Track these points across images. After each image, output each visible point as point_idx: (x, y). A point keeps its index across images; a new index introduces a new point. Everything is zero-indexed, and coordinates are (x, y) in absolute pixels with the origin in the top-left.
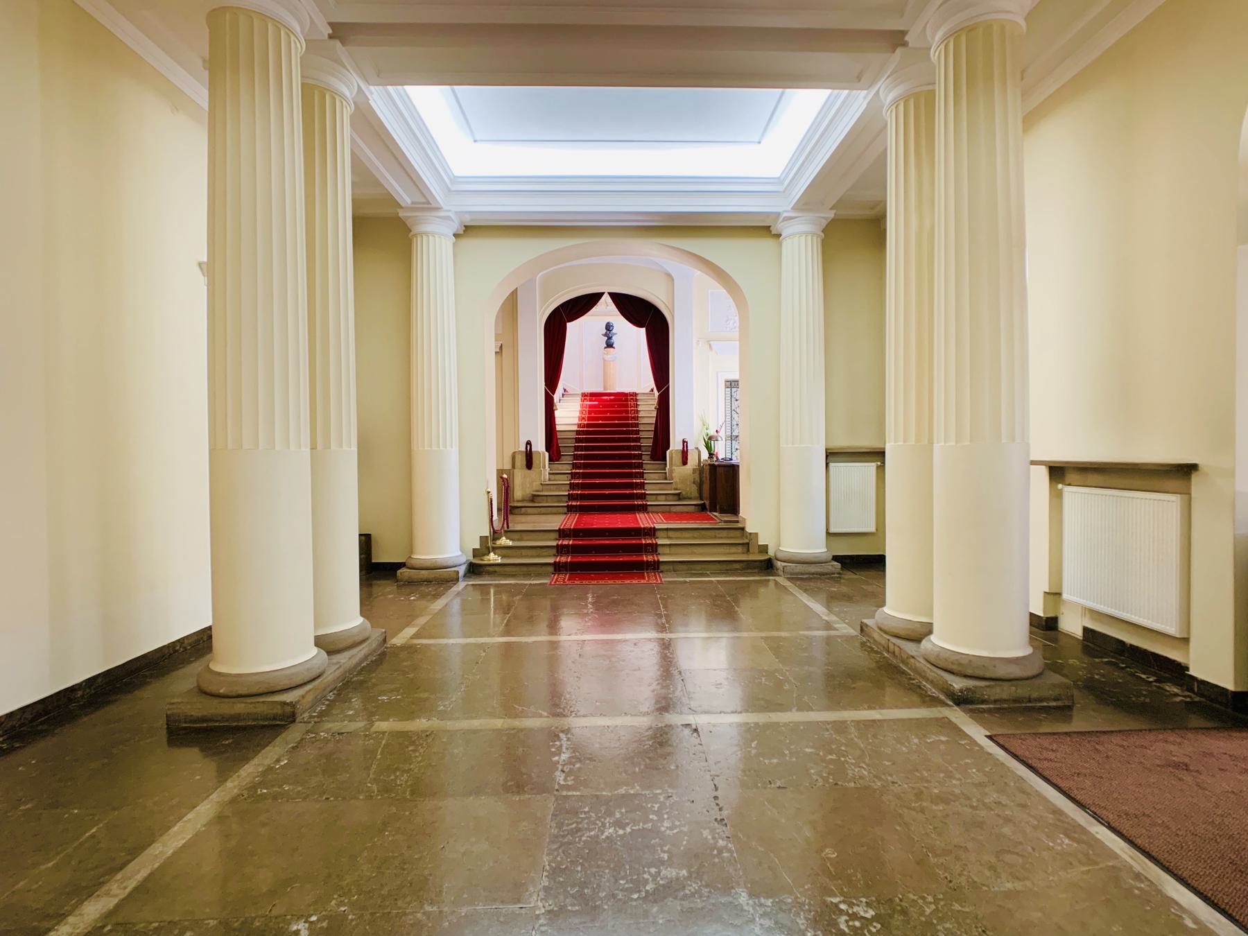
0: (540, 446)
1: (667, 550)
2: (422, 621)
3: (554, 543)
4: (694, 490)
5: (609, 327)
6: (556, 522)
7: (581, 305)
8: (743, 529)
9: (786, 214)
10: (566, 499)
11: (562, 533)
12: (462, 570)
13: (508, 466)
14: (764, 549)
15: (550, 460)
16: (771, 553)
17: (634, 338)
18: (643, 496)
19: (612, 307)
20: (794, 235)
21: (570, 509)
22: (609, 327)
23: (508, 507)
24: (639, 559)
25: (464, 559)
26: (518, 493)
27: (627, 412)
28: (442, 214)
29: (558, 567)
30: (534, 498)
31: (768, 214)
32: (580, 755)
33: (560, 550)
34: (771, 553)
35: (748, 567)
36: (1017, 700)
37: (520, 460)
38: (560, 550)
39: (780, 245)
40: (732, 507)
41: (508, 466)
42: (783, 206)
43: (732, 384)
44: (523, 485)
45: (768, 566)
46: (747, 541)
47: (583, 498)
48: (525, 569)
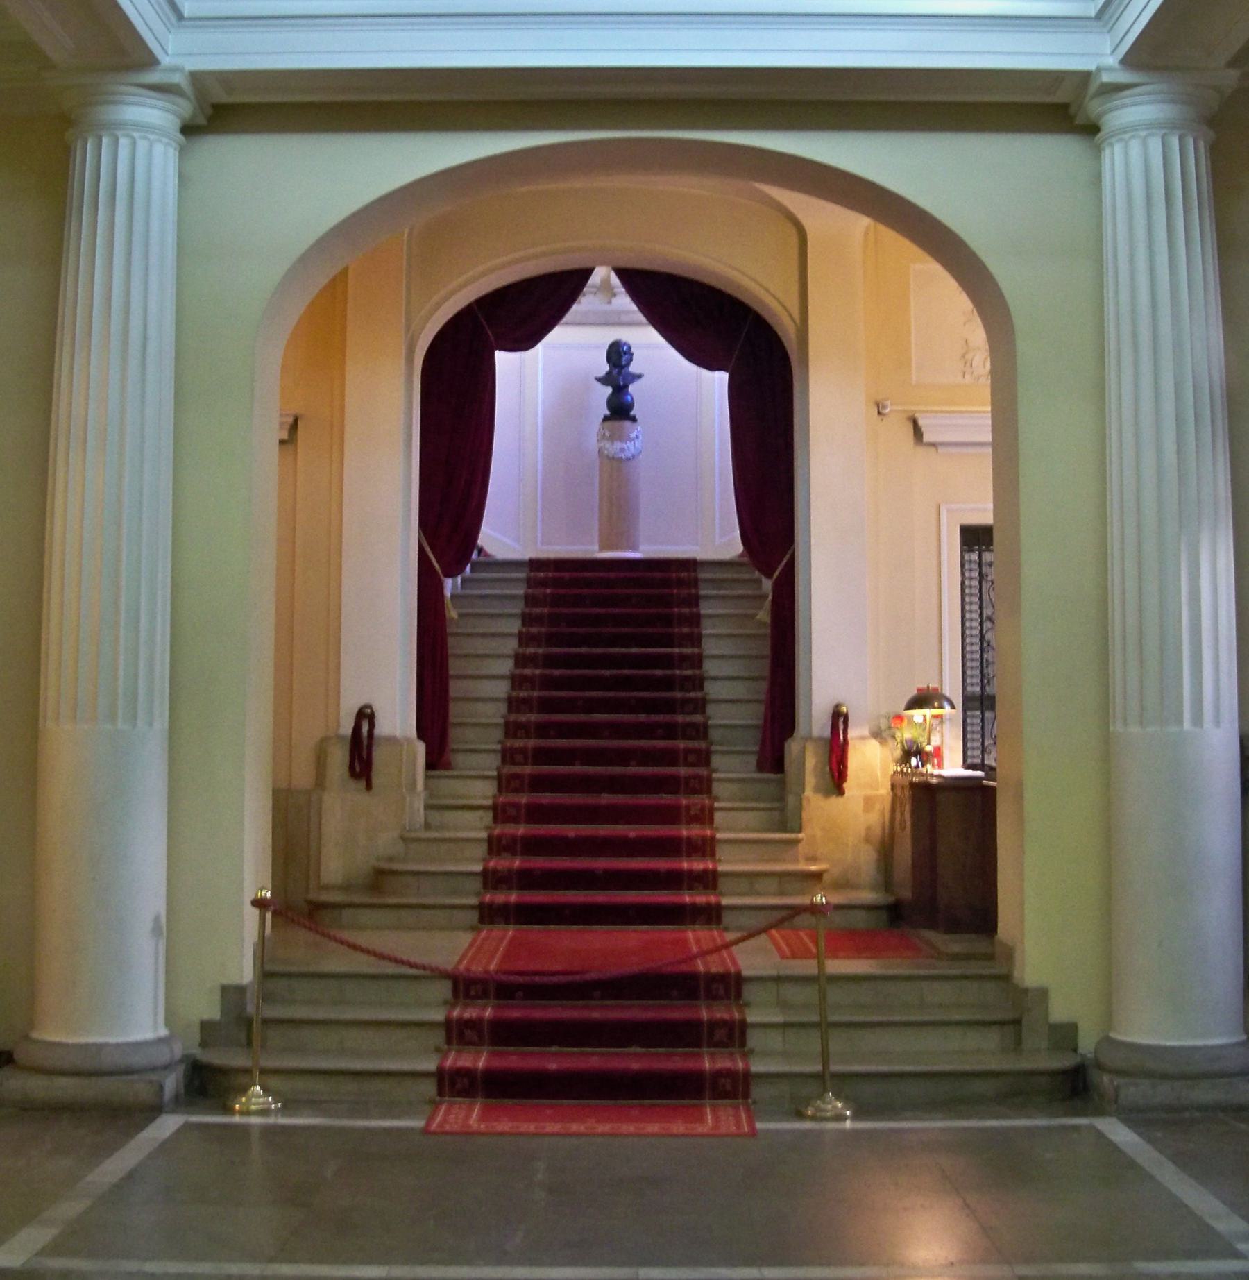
0: (398, 717)
1: (774, 1040)
2: (69, 1209)
3: (431, 1065)
4: (866, 859)
5: (618, 355)
6: (452, 946)
7: (530, 308)
8: (1006, 978)
9: (1106, 78)
10: (477, 884)
11: (465, 986)
12: (172, 1083)
13: (303, 777)
14: (1065, 1035)
15: (431, 765)
16: (1087, 1044)
17: (691, 397)
18: (709, 880)
19: (624, 302)
20: (1133, 128)
21: (489, 914)
22: (618, 355)
23: (297, 907)
24: (690, 1064)
25: (178, 1050)
26: (335, 865)
27: (668, 621)
28: (153, 77)
29: (453, 1084)
30: (380, 878)
31: (1056, 78)
32: (497, 972)
33: (458, 1033)
34: (1087, 1044)
35: (1017, 1091)
36: (1169, 1109)
37: (339, 758)
38: (458, 1033)
39: (1098, 151)
40: (981, 917)
41: (303, 777)
42: (1099, 54)
43: (975, 538)
44: (354, 832)
45: (1075, 1086)
46: (1016, 1012)
47: (535, 877)
48: (350, 1086)
